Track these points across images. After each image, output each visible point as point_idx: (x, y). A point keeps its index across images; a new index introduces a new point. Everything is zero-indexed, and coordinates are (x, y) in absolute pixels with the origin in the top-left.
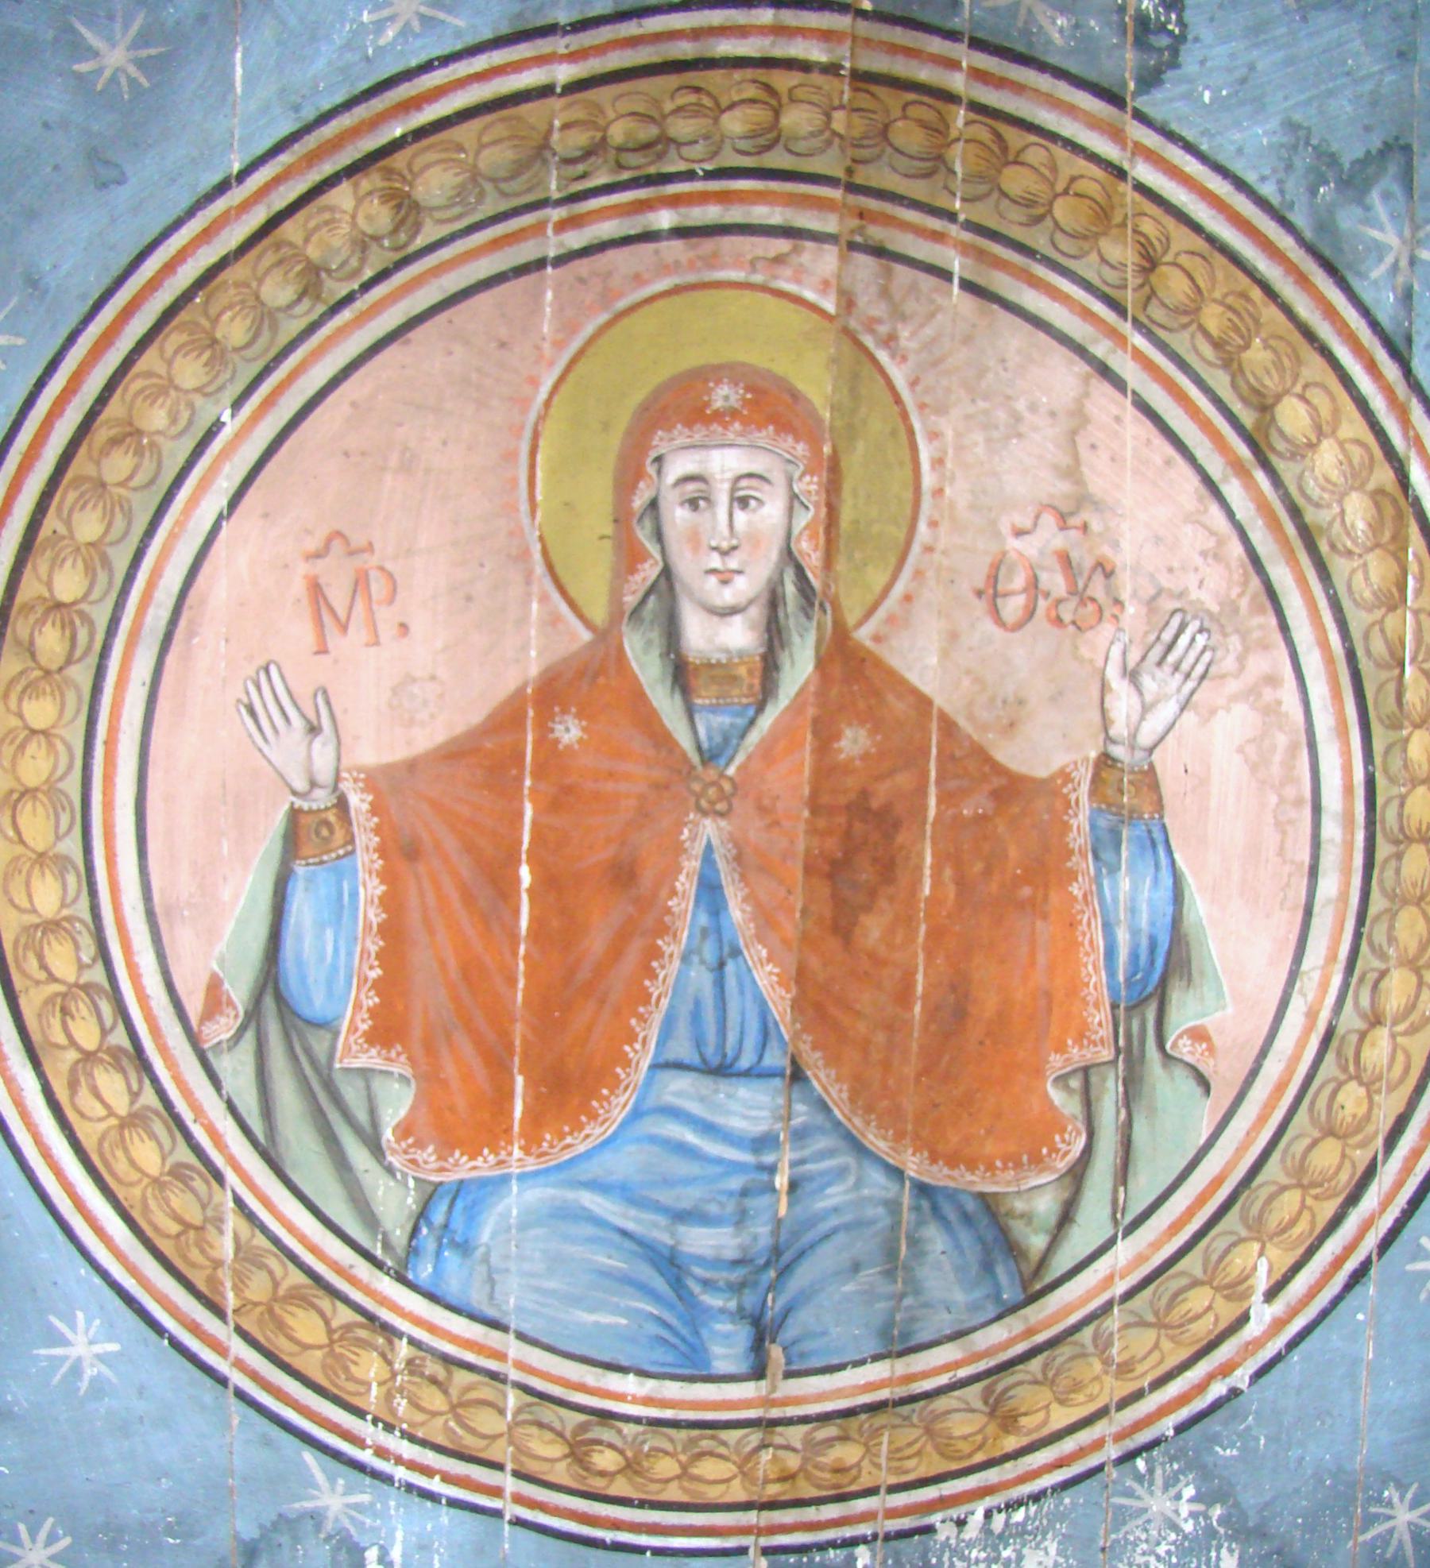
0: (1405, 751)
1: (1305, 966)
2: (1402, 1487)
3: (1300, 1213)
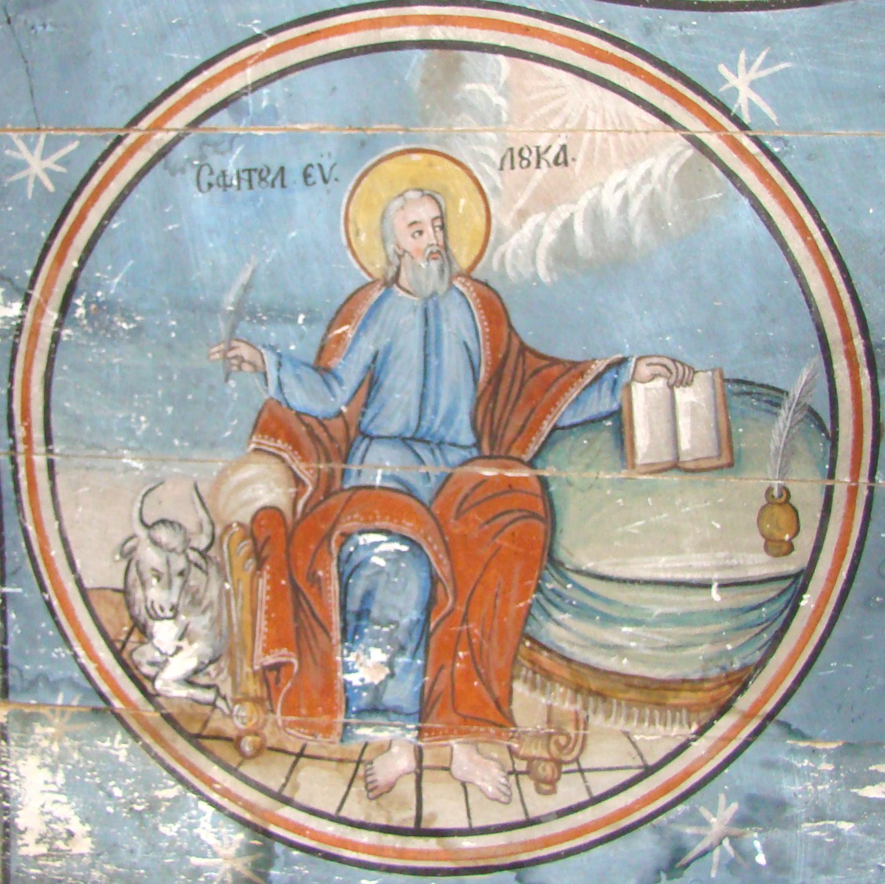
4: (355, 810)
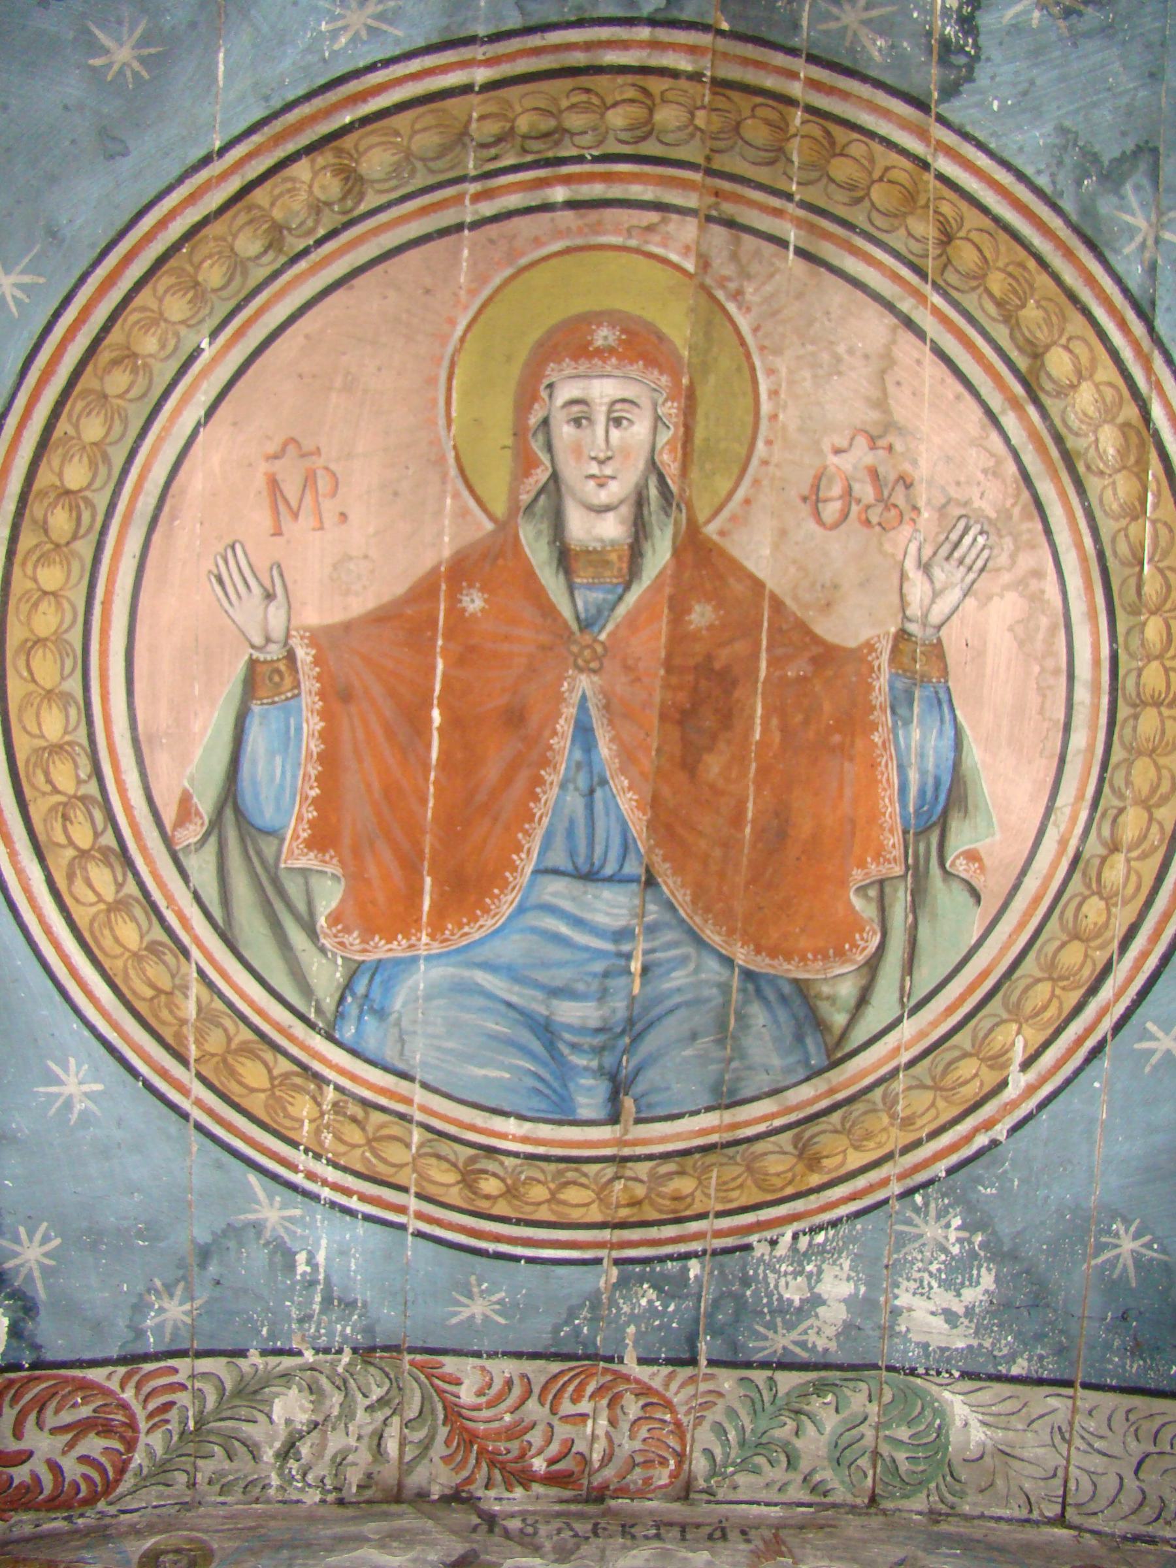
0: (1142, 632)
1: (1059, 802)
2: (1127, 1222)
3: (1050, 1001)
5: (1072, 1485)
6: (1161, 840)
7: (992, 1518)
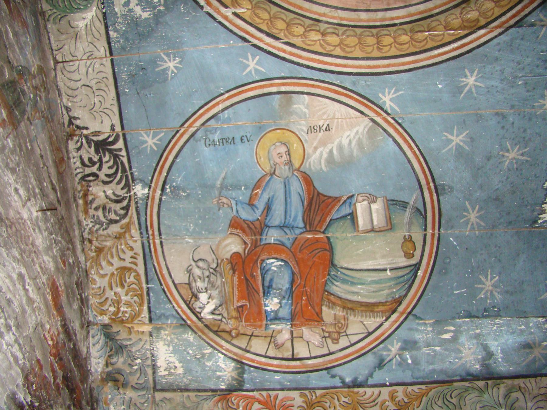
0: (404, 34)
1: (339, 12)
2: (180, 63)
3: (262, 19)
4: (271, 353)
5: (71, 63)
6: (328, 51)
7: (49, 36)
